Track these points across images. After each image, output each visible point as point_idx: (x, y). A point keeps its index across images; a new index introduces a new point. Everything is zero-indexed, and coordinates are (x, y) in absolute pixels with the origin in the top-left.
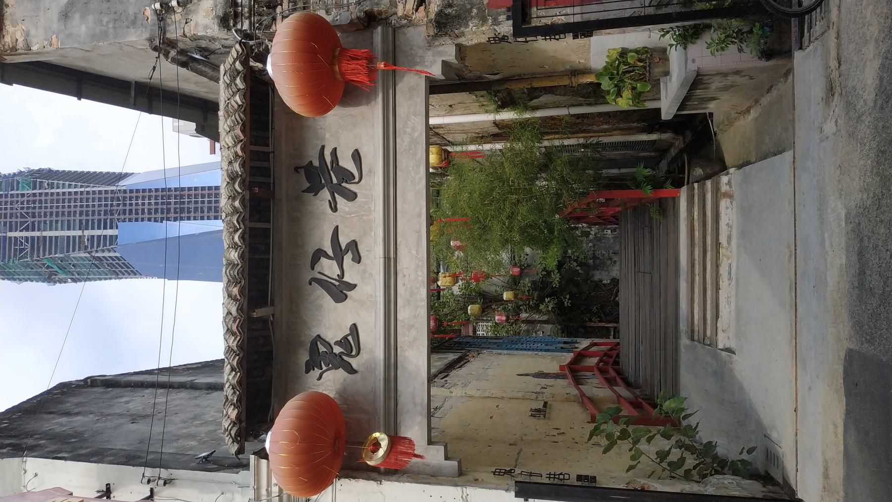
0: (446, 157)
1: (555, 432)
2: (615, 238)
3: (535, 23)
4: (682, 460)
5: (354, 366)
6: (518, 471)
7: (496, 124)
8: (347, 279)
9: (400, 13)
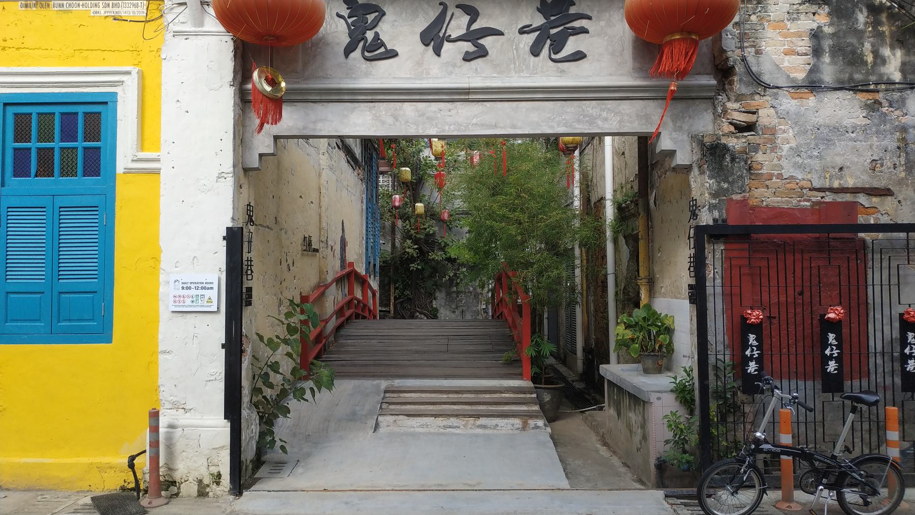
0: (569, 150)
1: (290, 262)
2: (478, 313)
3: (708, 248)
4: (271, 386)
5: (352, 55)
6: (252, 228)
7: (602, 199)
8: (447, 46)
9: (730, 105)
